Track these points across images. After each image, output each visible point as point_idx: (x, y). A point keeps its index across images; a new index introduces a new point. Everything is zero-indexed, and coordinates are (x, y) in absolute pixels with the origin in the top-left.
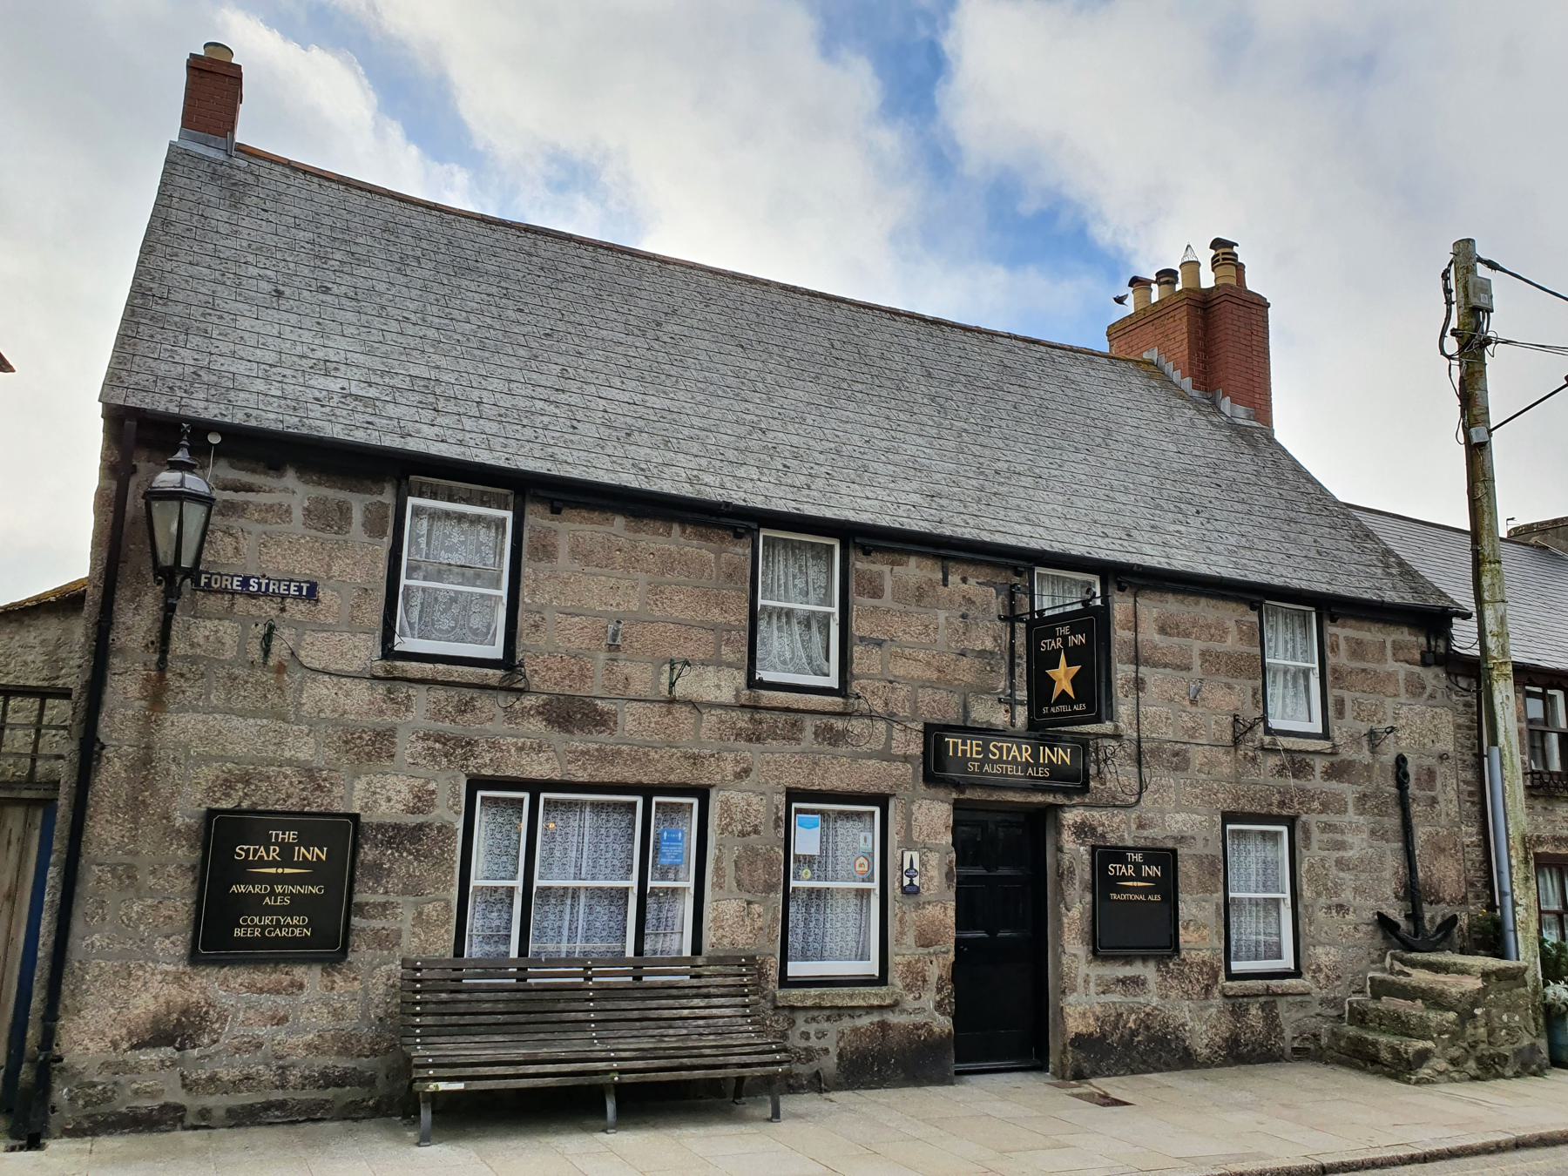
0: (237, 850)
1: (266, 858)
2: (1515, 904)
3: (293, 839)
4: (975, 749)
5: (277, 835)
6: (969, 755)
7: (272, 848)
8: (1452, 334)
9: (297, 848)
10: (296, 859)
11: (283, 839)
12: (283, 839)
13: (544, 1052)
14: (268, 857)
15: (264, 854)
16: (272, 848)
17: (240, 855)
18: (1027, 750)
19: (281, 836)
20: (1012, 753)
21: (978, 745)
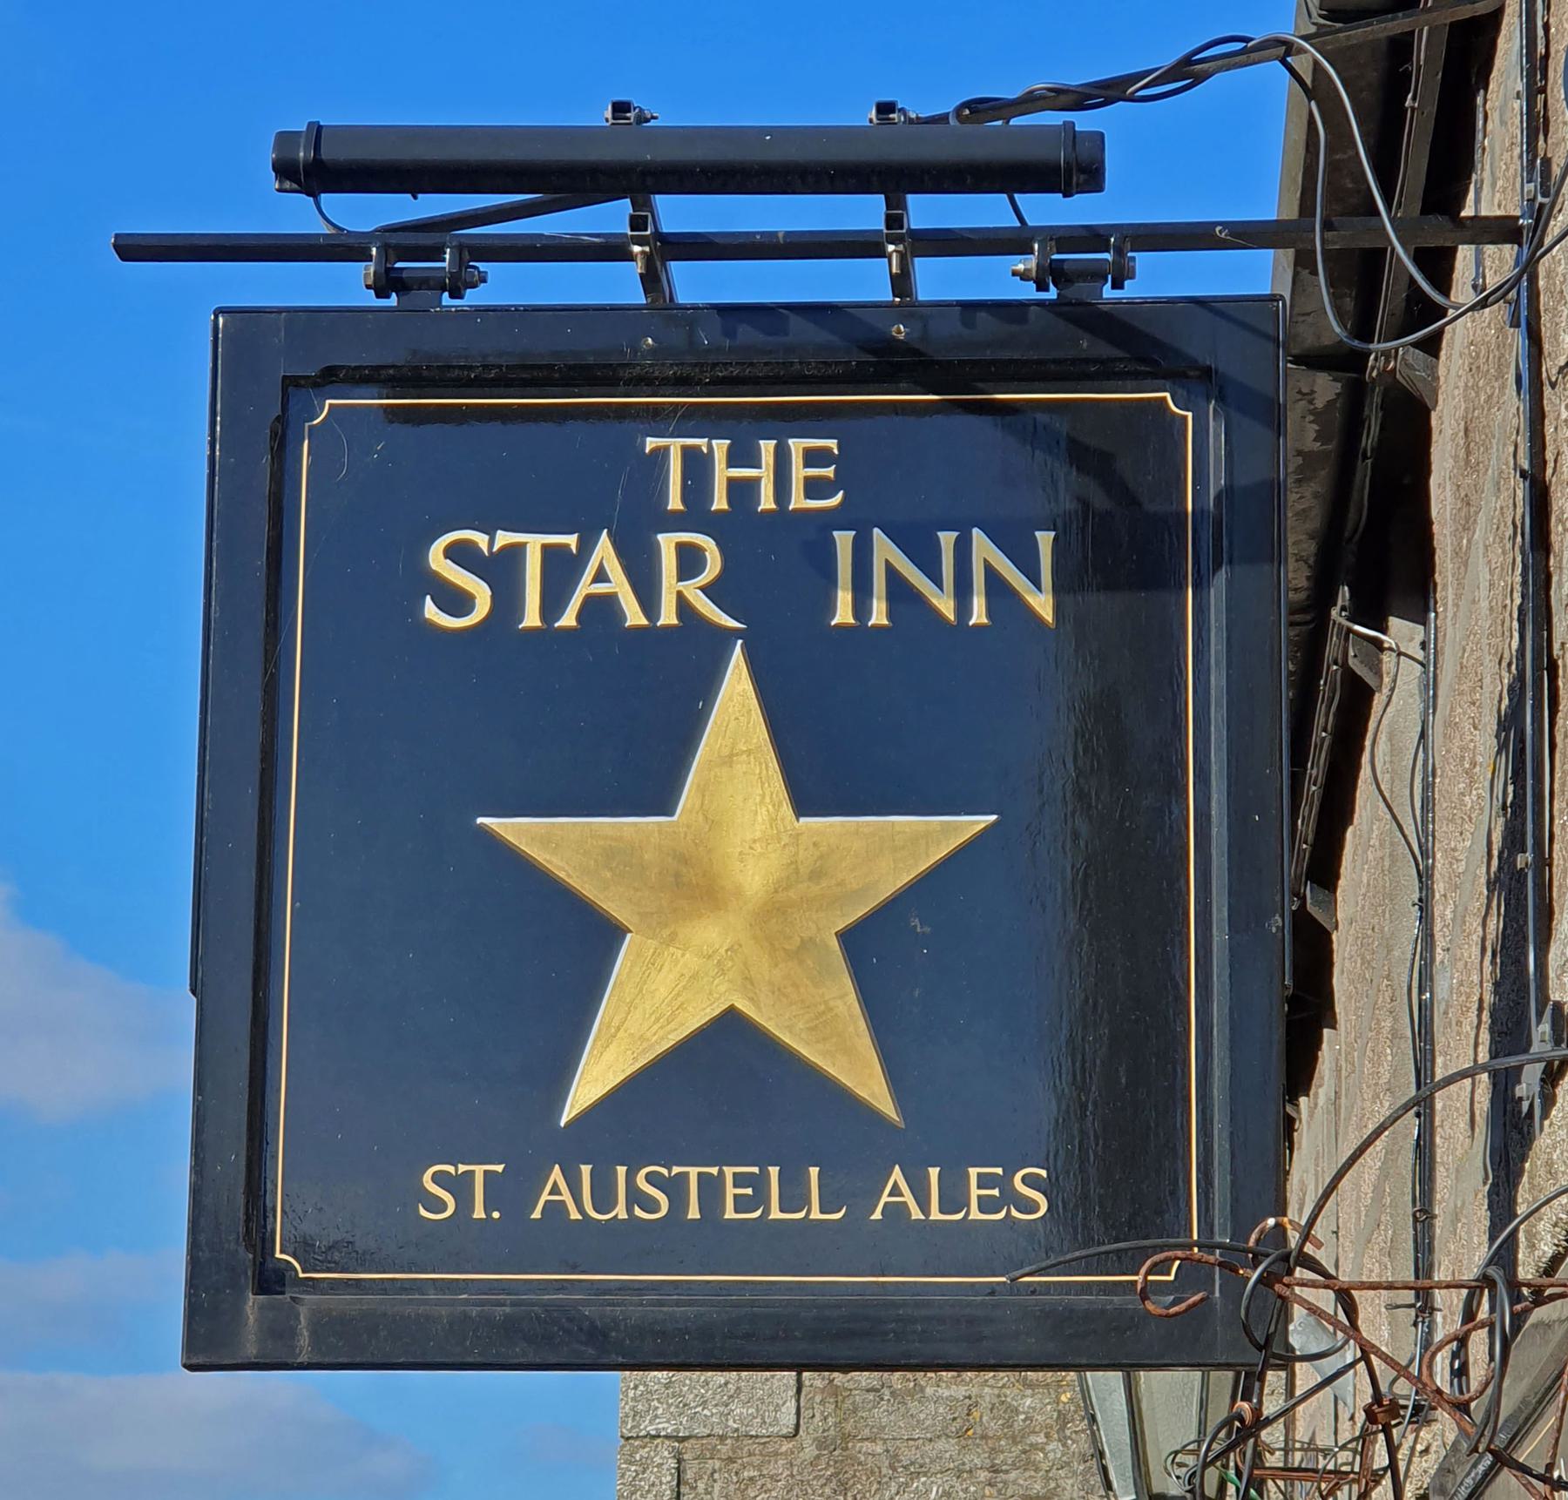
0: (437, 559)
1: (634, 616)
2: (1323, 1171)
3: (814, 488)
4: (799, 473)
5: (696, 466)
6: (767, 502)
7: (668, 542)
8: (1121, 287)
9: (844, 540)
10: (843, 614)
11: (742, 491)
12: (742, 491)
13: (1205, 549)
14: (649, 602)
15: (619, 585)
16: (668, 542)
17: (457, 602)
18: (690, 562)
19: (722, 473)
20: (585, 587)
21: (812, 457)
